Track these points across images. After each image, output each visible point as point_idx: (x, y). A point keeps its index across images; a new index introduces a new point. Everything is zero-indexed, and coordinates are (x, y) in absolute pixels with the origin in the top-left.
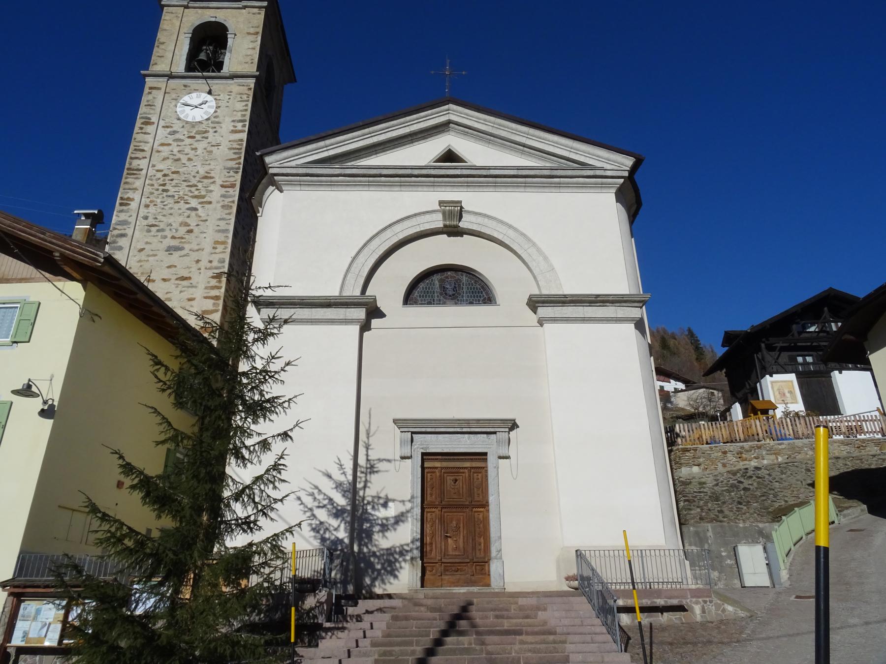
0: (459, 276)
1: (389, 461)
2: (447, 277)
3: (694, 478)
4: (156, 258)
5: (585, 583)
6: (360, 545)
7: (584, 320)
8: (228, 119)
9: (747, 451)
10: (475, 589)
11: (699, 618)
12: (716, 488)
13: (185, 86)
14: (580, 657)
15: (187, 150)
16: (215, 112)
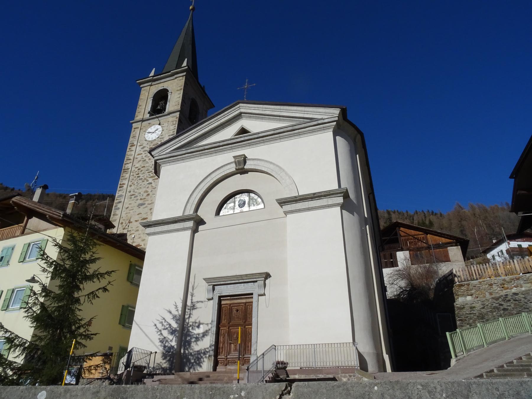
1: (202, 302)
3: (467, 304)
6: (184, 349)
9: (508, 282)
12: (482, 310)
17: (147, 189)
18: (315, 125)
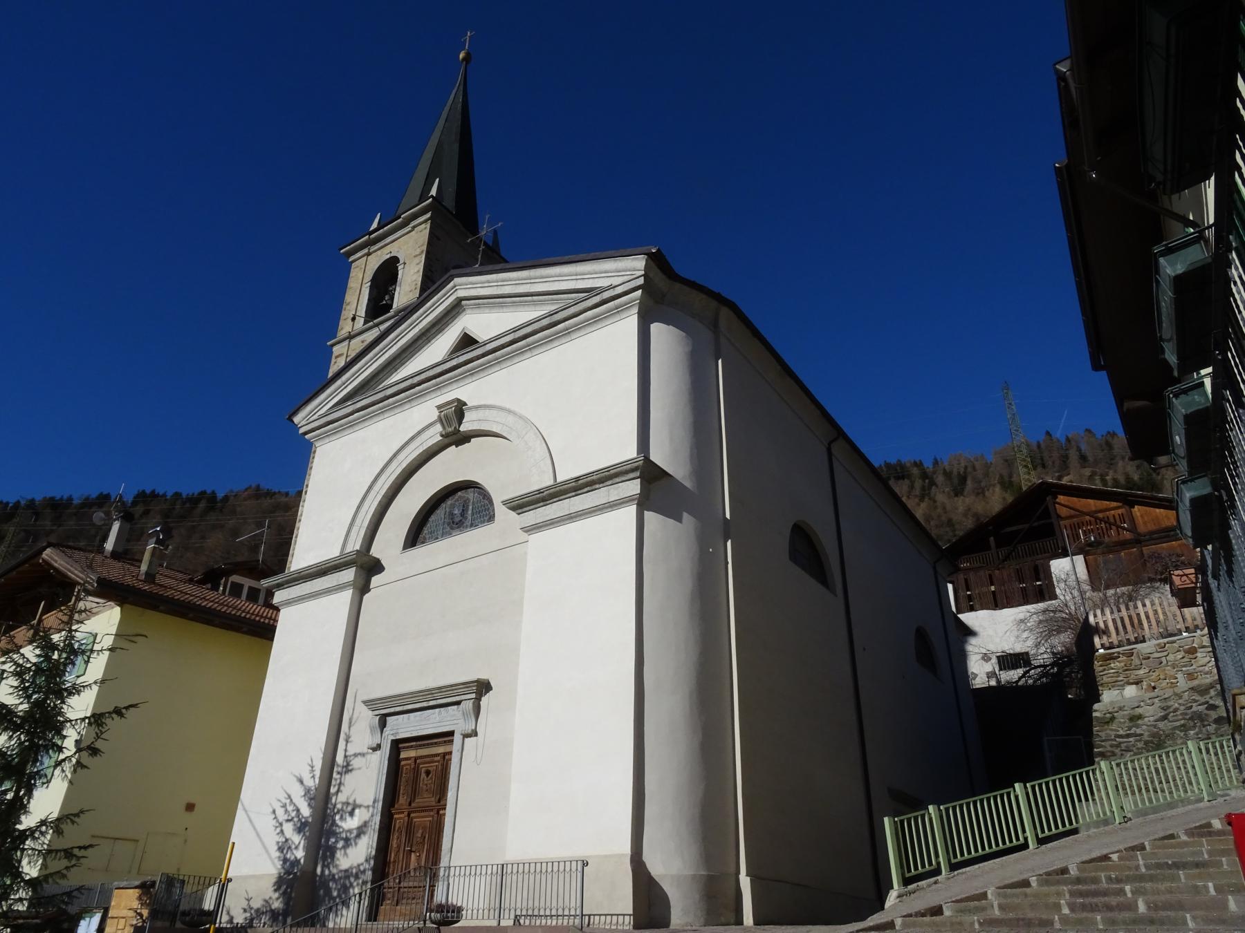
3: (1121, 709)
12: (1161, 725)
18: (593, 305)
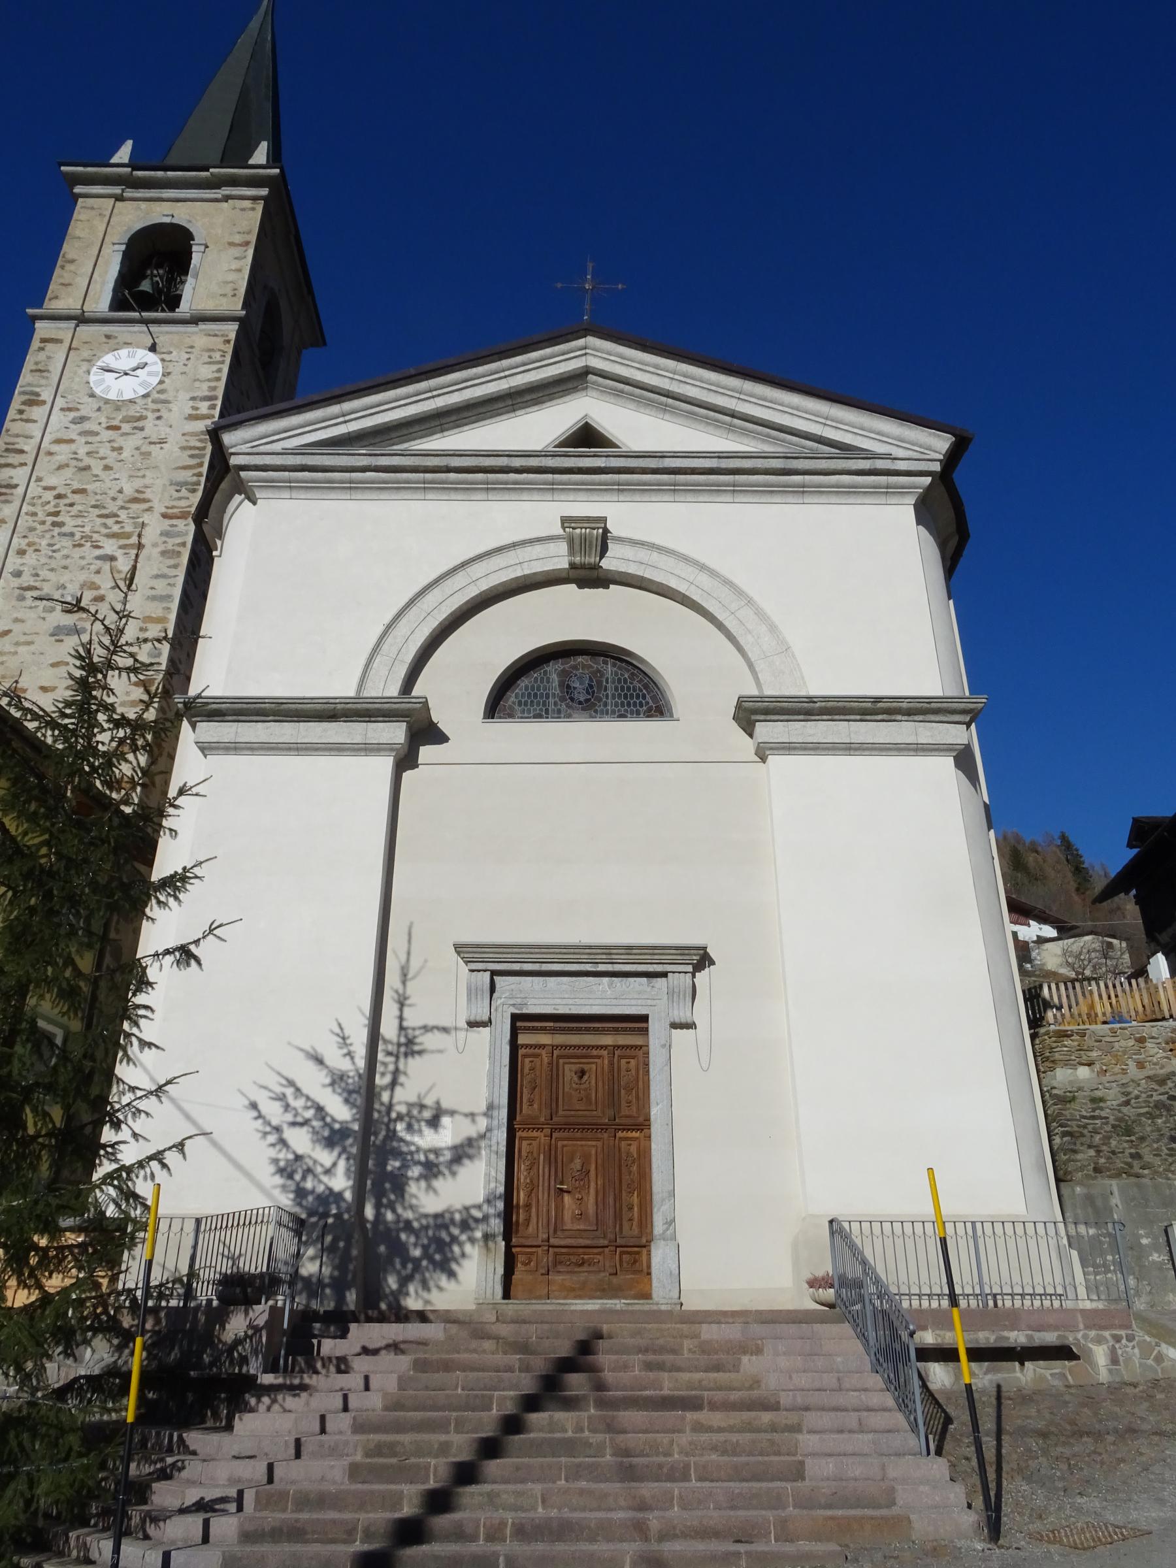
0: (598, 664)
1: (445, 1030)
2: (575, 667)
3: (1080, 1089)
4: (32, 648)
5: (851, 1293)
6: (378, 1206)
7: (850, 748)
8: (184, 396)
10: (618, 1304)
11: (1104, 1376)
12: (1125, 1110)
13: (108, 337)
14: (829, 1467)
15: (104, 451)
16: (161, 382)
17: (97, 579)
18: (869, 475)
